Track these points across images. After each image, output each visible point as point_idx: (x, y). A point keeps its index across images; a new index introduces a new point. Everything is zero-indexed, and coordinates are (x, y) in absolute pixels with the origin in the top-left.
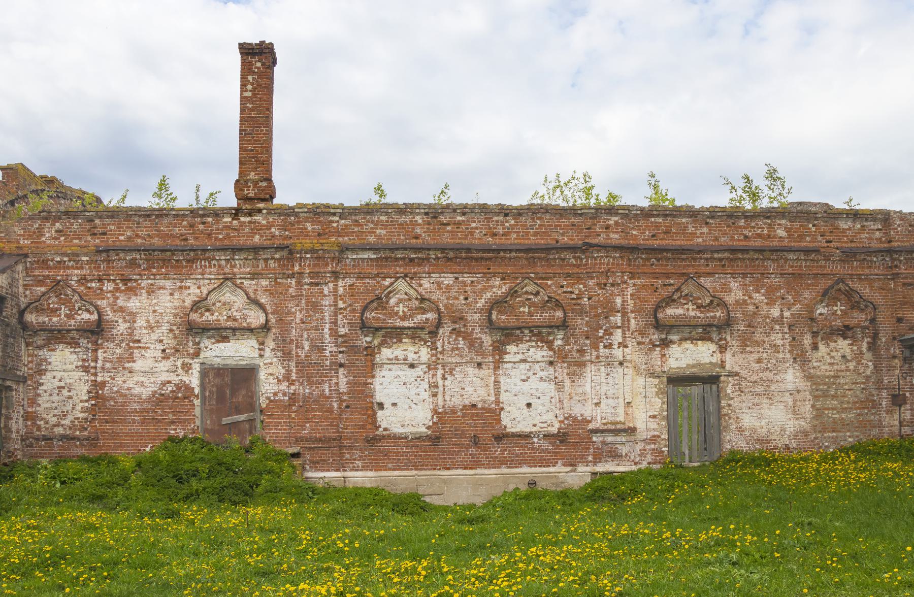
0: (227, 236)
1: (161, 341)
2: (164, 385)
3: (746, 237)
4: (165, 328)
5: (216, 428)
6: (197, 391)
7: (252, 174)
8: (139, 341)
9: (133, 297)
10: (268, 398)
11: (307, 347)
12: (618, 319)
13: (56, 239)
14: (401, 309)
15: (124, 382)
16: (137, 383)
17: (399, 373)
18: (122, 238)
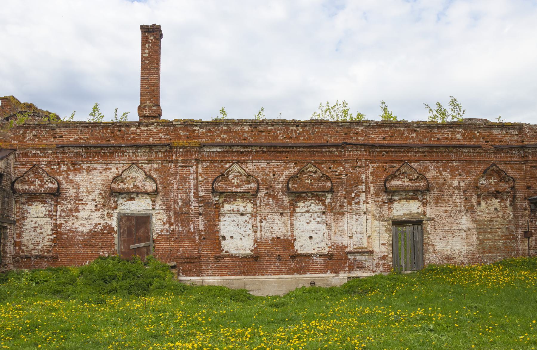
0: (134, 139)
1: (95, 200)
2: (96, 226)
3: (438, 139)
4: (97, 192)
5: (127, 251)
6: (116, 229)
7: (148, 102)
8: (81, 200)
9: (78, 174)
10: (157, 233)
11: (180, 204)
12: (363, 187)
13: (33, 140)
14: (235, 181)
15: (73, 224)
16: (81, 224)
17: (235, 219)
18: (71, 139)
